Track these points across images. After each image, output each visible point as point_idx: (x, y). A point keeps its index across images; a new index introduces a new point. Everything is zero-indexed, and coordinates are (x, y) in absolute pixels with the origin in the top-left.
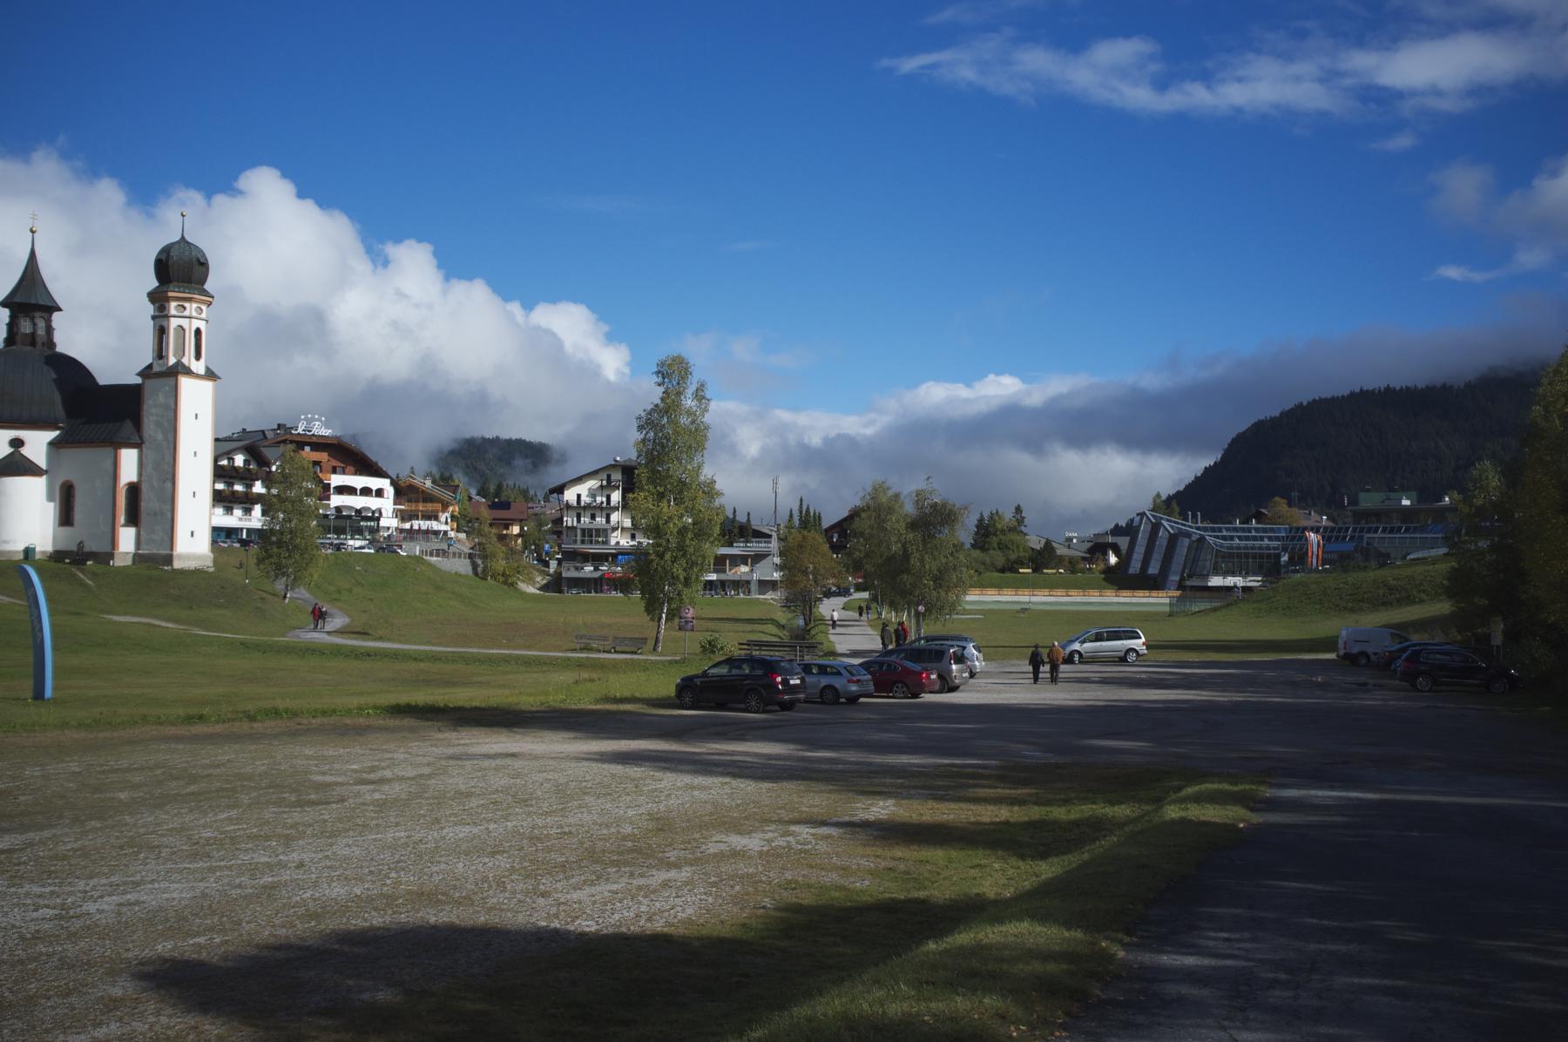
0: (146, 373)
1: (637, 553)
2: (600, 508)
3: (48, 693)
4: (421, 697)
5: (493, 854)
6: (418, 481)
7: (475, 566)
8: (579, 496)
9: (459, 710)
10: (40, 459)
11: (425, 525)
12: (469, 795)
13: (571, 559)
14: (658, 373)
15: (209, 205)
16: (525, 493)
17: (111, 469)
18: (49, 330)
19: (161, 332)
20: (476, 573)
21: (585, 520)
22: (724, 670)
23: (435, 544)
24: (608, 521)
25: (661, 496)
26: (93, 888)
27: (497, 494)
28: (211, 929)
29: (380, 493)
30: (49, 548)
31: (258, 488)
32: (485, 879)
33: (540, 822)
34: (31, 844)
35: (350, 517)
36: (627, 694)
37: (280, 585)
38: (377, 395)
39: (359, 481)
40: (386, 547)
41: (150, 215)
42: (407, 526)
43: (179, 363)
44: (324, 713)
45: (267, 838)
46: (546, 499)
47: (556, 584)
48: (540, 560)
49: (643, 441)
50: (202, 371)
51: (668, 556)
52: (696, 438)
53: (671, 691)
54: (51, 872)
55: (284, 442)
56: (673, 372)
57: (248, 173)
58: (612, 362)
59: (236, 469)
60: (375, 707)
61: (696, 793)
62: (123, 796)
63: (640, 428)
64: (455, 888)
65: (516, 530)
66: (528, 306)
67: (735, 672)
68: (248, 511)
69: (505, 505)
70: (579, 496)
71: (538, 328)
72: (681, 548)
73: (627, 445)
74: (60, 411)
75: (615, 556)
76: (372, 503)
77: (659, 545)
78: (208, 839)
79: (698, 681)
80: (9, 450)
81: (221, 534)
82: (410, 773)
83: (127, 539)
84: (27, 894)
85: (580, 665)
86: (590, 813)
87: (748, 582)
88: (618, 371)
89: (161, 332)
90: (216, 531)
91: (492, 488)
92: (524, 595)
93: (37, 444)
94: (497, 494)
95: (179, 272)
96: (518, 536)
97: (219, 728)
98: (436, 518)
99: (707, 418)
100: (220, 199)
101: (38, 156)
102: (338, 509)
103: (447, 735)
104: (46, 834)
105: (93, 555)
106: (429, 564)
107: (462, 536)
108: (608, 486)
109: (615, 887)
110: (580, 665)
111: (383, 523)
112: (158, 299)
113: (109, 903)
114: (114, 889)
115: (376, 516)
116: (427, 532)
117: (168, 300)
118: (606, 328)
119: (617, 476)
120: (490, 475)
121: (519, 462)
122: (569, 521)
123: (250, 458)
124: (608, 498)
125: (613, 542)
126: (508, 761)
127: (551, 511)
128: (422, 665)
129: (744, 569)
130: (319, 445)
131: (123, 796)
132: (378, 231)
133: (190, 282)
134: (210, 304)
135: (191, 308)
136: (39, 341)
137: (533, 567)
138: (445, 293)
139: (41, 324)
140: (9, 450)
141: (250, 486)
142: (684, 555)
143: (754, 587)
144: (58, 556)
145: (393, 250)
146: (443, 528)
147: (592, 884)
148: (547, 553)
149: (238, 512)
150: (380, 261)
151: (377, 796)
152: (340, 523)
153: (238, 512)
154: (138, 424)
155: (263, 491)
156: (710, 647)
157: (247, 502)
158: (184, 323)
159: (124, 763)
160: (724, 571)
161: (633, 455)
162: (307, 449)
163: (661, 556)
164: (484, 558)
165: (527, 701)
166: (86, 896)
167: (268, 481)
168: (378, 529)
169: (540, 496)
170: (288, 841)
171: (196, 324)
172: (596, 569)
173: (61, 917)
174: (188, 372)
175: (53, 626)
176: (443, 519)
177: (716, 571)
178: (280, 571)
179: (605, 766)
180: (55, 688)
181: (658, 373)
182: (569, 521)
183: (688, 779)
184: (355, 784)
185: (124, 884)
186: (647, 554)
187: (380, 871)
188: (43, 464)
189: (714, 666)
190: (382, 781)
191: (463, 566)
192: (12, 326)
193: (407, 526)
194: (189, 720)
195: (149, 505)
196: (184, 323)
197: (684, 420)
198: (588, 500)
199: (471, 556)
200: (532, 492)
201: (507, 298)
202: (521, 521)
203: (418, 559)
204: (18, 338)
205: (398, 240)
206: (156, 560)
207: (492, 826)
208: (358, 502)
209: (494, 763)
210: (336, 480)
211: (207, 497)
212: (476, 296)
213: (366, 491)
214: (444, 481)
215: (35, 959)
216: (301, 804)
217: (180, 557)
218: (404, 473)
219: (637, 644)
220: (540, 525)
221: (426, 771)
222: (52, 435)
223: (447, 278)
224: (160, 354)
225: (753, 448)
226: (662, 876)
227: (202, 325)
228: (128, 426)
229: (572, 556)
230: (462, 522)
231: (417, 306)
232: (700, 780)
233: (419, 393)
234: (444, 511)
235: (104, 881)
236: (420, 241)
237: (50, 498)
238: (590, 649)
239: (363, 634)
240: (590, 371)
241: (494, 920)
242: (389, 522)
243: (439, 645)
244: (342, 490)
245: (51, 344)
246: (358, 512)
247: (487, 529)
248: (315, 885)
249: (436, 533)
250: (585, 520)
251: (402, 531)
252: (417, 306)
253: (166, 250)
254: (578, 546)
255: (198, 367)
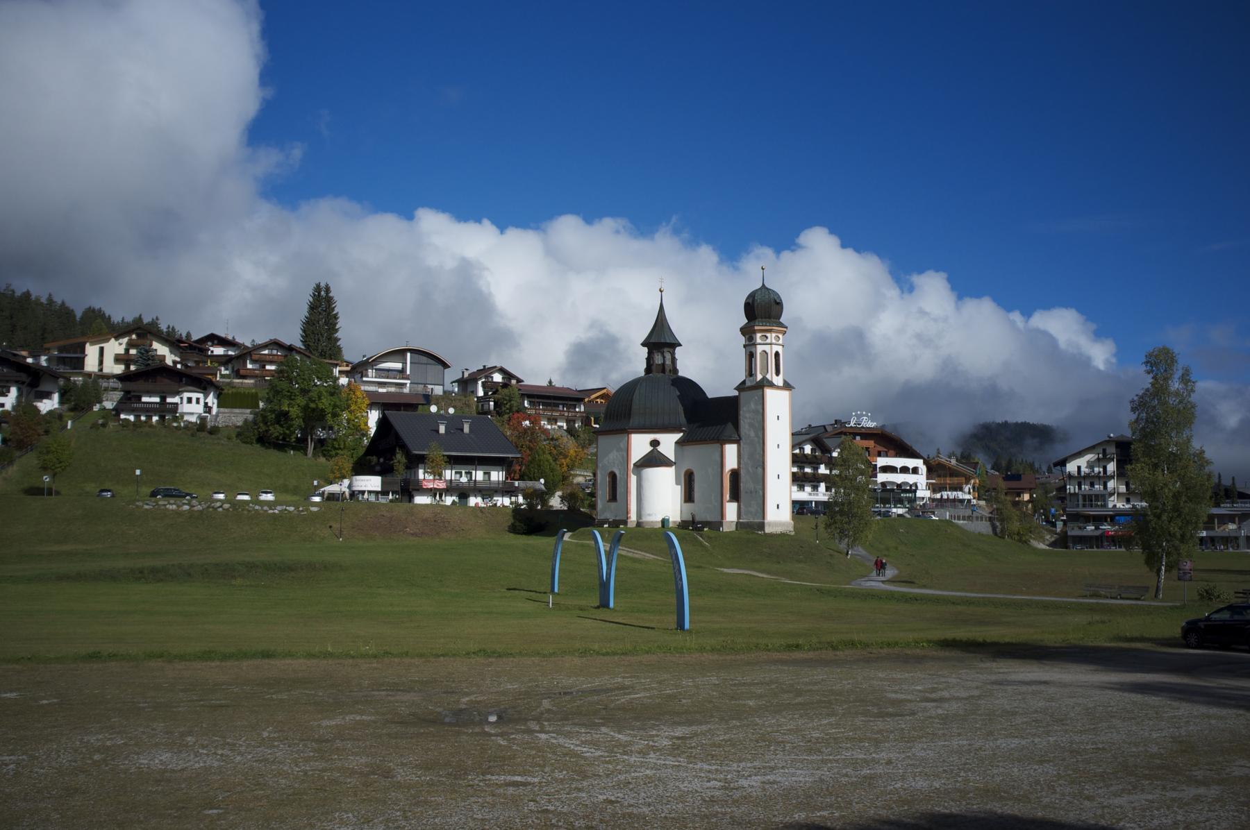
0: (741, 387)
1: (1134, 514)
2: (1098, 476)
3: (687, 626)
4: (962, 634)
5: (1041, 762)
6: (943, 459)
7: (994, 528)
8: (1079, 468)
9: (994, 644)
10: (671, 455)
11: (952, 495)
12: (1014, 714)
13: (1075, 518)
14: (1146, 363)
15: (778, 257)
16: (1032, 466)
17: (719, 459)
18: (674, 360)
19: (751, 356)
20: (995, 534)
21: (1085, 487)
22: (1226, 616)
23: (962, 511)
24: (1105, 487)
25: (1156, 466)
26: (744, 769)
27: (1008, 468)
28: (831, 806)
29: (915, 471)
30: (679, 520)
31: (823, 470)
32: (1037, 782)
33: (1077, 738)
34: (696, 735)
35: (892, 490)
36: (1136, 634)
37: (843, 546)
38: (912, 394)
39: (899, 462)
40: (920, 512)
41: (736, 269)
42: (938, 496)
43: (764, 378)
44: (889, 645)
45: (861, 740)
46: (1049, 470)
47: (1063, 541)
48: (1048, 521)
49: (1137, 421)
50: (781, 384)
51: (1164, 517)
52: (1185, 415)
53: (1177, 632)
54: (713, 756)
55: (841, 433)
56: (1160, 362)
57: (806, 232)
58: (1100, 355)
59: (806, 456)
60: (929, 641)
61: (1213, 722)
62: (751, 703)
63: (1133, 410)
64: (1013, 787)
65: (1026, 497)
66: (1027, 314)
67: (1236, 617)
68: (815, 488)
69: (1017, 477)
70: (1079, 468)
71: (1038, 331)
72: (1177, 509)
73: (1123, 423)
74: (683, 419)
75: (1112, 518)
76: (910, 478)
77: (1157, 508)
78: (817, 739)
79: (1202, 625)
80: (650, 449)
81: (800, 508)
82: (964, 694)
83: (731, 511)
84: (701, 770)
85: (1092, 609)
86: (1118, 733)
87: (1236, 538)
88: (1107, 361)
89: (751, 356)
90: (794, 503)
91: (1004, 464)
92: (1035, 550)
93: (668, 443)
94: (1008, 468)
95: (762, 311)
96: (1028, 502)
97: (811, 655)
98: (961, 489)
99: (1194, 398)
100: (786, 255)
101: (657, 236)
102: (883, 484)
103: (988, 664)
104: (704, 728)
105: (706, 524)
106: (957, 526)
107: (982, 503)
108: (1103, 460)
109: (1150, 797)
110: (1092, 609)
111: (919, 494)
112: (748, 332)
113: (756, 781)
114: (758, 771)
115: (913, 489)
116: (954, 500)
117: (755, 332)
118: (1093, 326)
119: (1112, 450)
120: (1003, 452)
121: (1030, 442)
122: (1071, 488)
123: (818, 445)
124: (1105, 468)
125: (1110, 505)
126: (1042, 687)
127: (1055, 481)
128: (960, 608)
129: (1232, 526)
130: (867, 434)
131: (751, 703)
132: (904, 267)
133: (770, 318)
134: (784, 333)
135: (771, 337)
136: (667, 369)
137: (1042, 527)
138: (958, 308)
139: (668, 356)
140: (650, 449)
141: (816, 469)
142: (1179, 516)
143: (1242, 542)
144: (683, 525)
145: (917, 279)
146: (967, 497)
147: (1129, 793)
148: (1053, 516)
149: (808, 489)
150: (907, 288)
151: (940, 711)
152: (886, 495)
153: (808, 489)
154: (736, 426)
155: (827, 472)
156: (1207, 595)
157: (814, 480)
158: (767, 348)
159: (748, 679)
160: (1213, 529)
161: (1128, 433)
162: (858, 438)
163: (1159, 517)
164: (1002, 520)
165: (1050, 638)
166: (739, 775)
167: (831, 464)
168: (915, 499)
169: (1044, 469)
170: (877, 743)
171: (775, 348)
172: (1097, 528)
173: (726, 788)
174: (771, 385)
175: (688, 576)
176: (966, 490)
177: (1205, 529)
178: (843, 534)
179: (1126, 694)
180: (690, 622)
181: (1146, 363)
182: (1071, 488)
183: (1203, 709)
184: (921, 701)
185: (764, 768)
186: (1145, 515)
187: (952, 771)
188: (672, 457)
189: (1217, 612)
190: (942, 700)
191: (984, 527)
192: (649, 360)
193: (938, 496)
194: (789, 648)
195: (747, 485)
196: (767, 348)
197: (1172, 401)
198: (1087, 471)
199: (990, 519)
200: (1037, 466)
201: (1008, 308)
202: (1030, 490)
203: (949, 522)
204: (654, 368)
205: (921, 271)
206: (752, 527)
207: (1037, 740)
208: (898, 478)
209: (1030, 689)
210: (881, 462)
211: (787, 478)
212: (983, 312)
213: (905, 470)
214: (965, 458)
215: (715, 816)
216: (882, 715)
217: (770, 524)
218: (933, 454)
219: (1140, 592)
220: (1047, 492)
221: (976, 693)
222: (678, 436)
223: (960, 297)
224: (751, 372)
225: (1233, 421)
226: (1192, 791)
227: (780, 349)
228: (730, 426)
229: (1074, 518)
230: (981, 492)
231: (935, 320)
232: (1214, 710)
233: (944, 390)
234: (967, 483)
235: (749, 765)
236: (937, 271)
237: (677, 483)
238: (1099, 596)
239: (910, 583)
240: (1084, 362)
241: (1051, 815)
242: (923, 493)
243: (972, 591)
244: (886, 469)
245: (675, 370)
246: (899, 486)
247: (1003, 497)
248: (903, 778)
249: (962, 501)
250: (1085, 487)
251: (933, 500)
252: (935, 320)
253: (752, 296)
254: (1080, 509)
255: (778, 381)
